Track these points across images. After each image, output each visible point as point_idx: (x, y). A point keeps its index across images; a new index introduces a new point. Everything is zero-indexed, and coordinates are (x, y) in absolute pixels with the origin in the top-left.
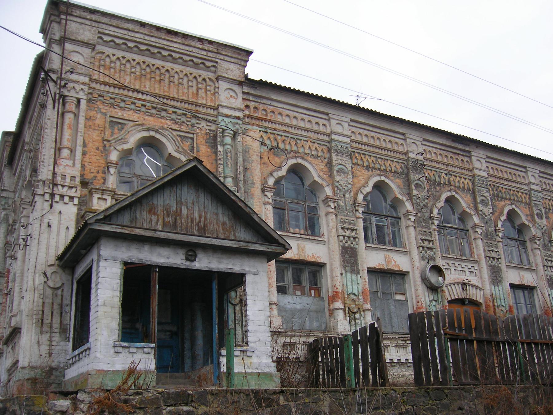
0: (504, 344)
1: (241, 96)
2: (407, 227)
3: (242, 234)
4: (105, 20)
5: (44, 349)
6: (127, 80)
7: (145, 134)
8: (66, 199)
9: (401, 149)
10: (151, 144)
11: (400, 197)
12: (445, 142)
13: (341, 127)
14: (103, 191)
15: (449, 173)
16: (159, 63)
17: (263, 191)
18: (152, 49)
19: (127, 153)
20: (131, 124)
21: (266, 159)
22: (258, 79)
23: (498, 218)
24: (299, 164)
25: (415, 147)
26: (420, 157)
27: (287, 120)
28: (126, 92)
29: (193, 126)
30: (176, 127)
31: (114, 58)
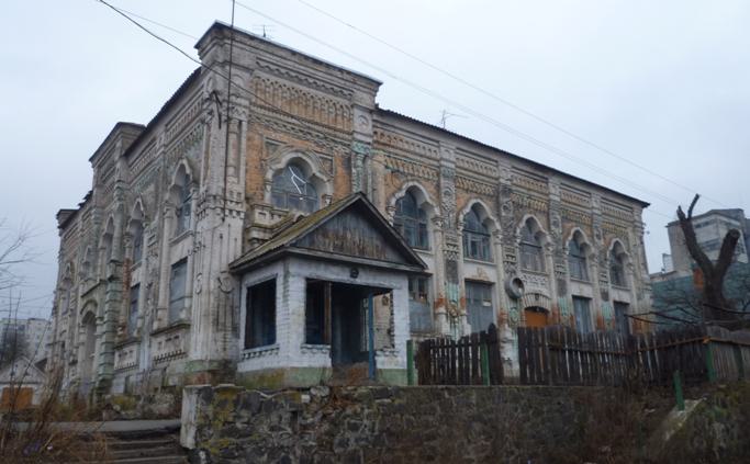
0: (576, 352)
1: (371, 123)
2: (496, 244)
3: (391, 255)
4: (262, 46)
5: (220, 344)
6: (279, 104)
7: (294, 155)
8: (234, 214)
9: (494, 175)
10: (297, 164)
11: (492, 217)
12: (524, 168)
13: (448, 154)
14: (263, 207)
15: (529, 197)
16: (305, 89)
17: (387, 209)
18: (318, 82)
19: (278, 172)
20: (283, 145)
21: (389, 179)
22: (385, 109)
23: (566, 237)
24: (415, 187)
25: (505, 174)
26: (509, 183)
27: (406, 147)
28: (278, 116)
29: (332, 148)
30: (318, 149)
31: (269, 83)
